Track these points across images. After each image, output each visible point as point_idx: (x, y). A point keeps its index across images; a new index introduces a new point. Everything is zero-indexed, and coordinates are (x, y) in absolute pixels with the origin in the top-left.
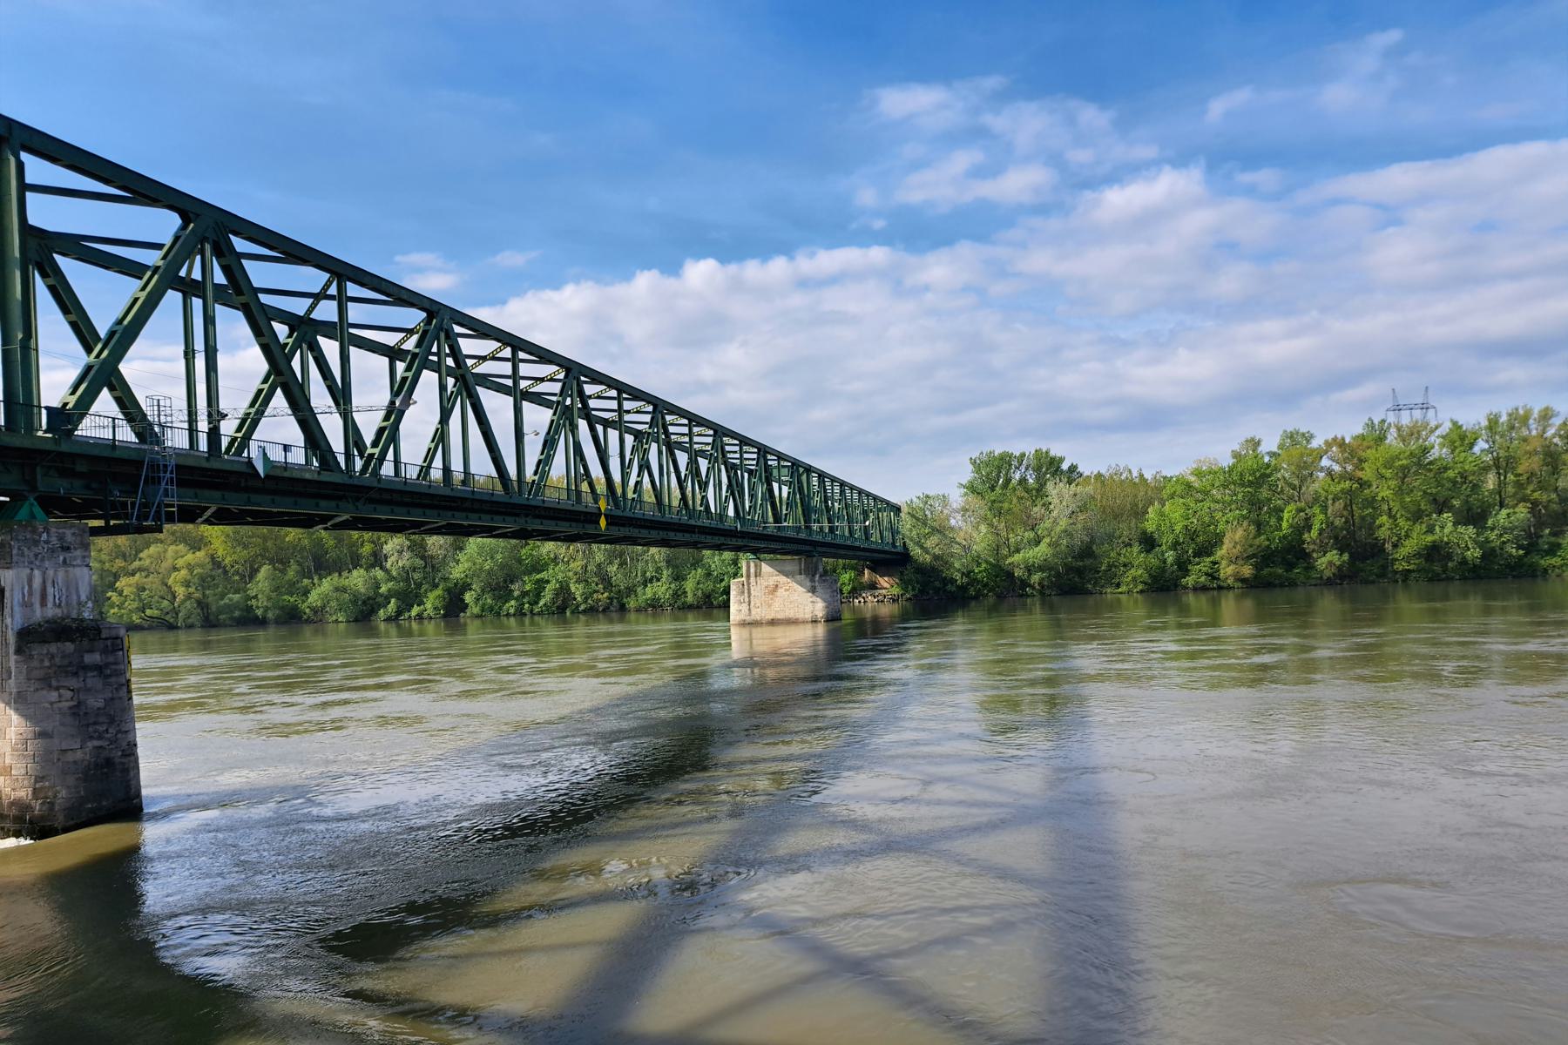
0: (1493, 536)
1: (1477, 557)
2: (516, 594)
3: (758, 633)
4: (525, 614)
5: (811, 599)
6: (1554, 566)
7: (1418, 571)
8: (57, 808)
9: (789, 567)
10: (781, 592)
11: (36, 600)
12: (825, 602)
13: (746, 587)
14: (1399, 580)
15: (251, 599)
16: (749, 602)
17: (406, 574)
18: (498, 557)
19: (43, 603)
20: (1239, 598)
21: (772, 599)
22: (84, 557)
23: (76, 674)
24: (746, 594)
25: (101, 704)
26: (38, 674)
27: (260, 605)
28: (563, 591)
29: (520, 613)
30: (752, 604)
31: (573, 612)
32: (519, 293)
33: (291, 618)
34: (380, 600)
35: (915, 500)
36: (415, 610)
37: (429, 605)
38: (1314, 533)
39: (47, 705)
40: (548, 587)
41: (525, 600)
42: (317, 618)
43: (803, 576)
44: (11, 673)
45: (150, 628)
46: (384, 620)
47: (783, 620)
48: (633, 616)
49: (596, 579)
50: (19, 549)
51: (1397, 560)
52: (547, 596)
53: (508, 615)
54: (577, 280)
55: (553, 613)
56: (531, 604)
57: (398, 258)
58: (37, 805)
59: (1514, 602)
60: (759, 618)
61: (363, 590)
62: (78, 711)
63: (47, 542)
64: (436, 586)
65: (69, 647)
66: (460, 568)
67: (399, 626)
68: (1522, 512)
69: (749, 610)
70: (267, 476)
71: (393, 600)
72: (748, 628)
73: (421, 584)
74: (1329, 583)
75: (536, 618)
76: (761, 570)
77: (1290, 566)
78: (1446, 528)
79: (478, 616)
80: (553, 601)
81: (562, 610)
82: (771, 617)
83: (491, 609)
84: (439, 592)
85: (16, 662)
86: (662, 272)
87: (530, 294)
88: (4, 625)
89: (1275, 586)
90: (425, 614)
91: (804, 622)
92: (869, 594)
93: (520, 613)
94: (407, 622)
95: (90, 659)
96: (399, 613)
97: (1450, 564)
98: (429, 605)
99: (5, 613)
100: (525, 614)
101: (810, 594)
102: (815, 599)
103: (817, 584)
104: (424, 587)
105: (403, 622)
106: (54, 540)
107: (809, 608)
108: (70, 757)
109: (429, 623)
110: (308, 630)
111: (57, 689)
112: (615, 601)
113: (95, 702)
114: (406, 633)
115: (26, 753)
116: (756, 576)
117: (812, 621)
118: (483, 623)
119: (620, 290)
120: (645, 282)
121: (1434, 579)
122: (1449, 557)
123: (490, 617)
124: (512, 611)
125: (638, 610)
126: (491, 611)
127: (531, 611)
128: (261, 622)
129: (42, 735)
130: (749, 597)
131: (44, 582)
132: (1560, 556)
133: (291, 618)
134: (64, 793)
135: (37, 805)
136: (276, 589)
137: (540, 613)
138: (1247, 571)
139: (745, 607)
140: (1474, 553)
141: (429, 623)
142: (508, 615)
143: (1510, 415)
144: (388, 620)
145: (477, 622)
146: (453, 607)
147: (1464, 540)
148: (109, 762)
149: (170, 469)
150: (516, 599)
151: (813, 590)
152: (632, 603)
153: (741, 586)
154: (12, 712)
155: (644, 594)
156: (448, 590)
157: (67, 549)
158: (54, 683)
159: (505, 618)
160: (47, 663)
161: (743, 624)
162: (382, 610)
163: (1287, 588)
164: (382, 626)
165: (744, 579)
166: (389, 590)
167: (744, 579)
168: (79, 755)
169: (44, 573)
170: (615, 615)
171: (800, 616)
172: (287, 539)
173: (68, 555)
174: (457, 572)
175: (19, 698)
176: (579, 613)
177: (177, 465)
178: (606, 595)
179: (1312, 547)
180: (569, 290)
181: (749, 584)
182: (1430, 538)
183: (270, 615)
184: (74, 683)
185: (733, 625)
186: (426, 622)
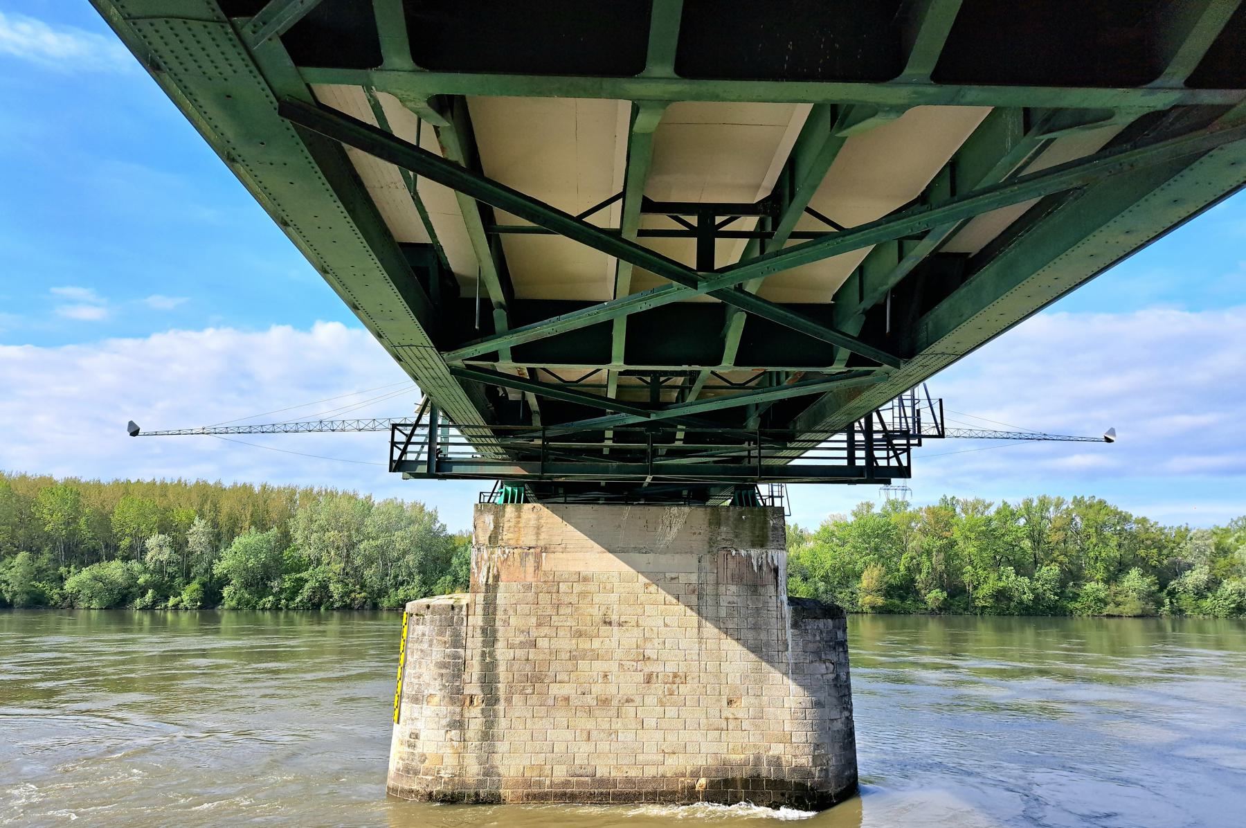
0: (1038, 585)
1: (1030, 600)
2: (274, 590)
4: (281, 609)
6: (1077, 609)
7: (991, 608)
8: (830, 774)
14: (978, 614)
17: (160, 569)
18: (262, 557)
20: (874, 619)
26: (811, 647)
27: (10, 589)
29: (276, 608)
31: (327, 609)
32: (163, 329)
33: (37, 603)
36: (172, 601)
38: (923, 575)
39: (819, 676)
40: (307, 586)
41: (283, 596)
42: (69, 604)
44: (788, 645)
46: (139, 609)
48: (385, 614)
51: (978, 598)
52: (306, 592)
53: (264, 609)
54: (217, 326)
55: (308, 609)
56: (287, 600)
57: (54, 290)
59: (1054, 631)
66: (224, 564)
67: (153, 616)
68: (1056, 569)
71: (150, 591)
73: (174, 577)
74: (932, 612)
75: (291, 613)
77: (903, 599)
78: (1009, 578)
79: (234, 609)
81: (317, 607)
83: (248, 603)
85: (793, 635)
86: (295, 328)
87: (171, 332)
88: (779, 601)
89: (895, 613)
90: (182, 605)
93: (276, 608)
94: (162, 612)
96: (155, 603)
97: (1012, 604)
98: (185, 597)
99: (779, 589)
100: (281, 609)
104: (177, 580)
105: (159, 611)
112: (369, 600)
115: (805, 721)
120: (278, 335)
121: (1001, 614)
122: (1010, 599)
124: (268, 605)
125: (389, 609)
127: (287, 606)
129: (818, 704)
132: (1080, 602)
133: (37, 603)
134: (833, 762)
135: (816, 772)
137: (294, 609)
138: (880, 601)
140: (1028, 597)
143: (1040, 501)
144: (144, 609)
145: (233, 615)
146: (210, 598)
147: (1022, 587)
150: (274, 595)
152: (385, 603)
154: (790, 682)
155: (397, 596)
158: (823, 657)
159: (260, 612)
162: (138, 600)
163: (903, 615)
164: (137, 615)
166: (146, 582)
170: (367, 613)
172: (46, 529)
174: (218, 569)
175: (796, 669)
179: (920, 585)
180: (209, 332)
182: (1001, 584)
183: (18, 599)
186: (181, 613)
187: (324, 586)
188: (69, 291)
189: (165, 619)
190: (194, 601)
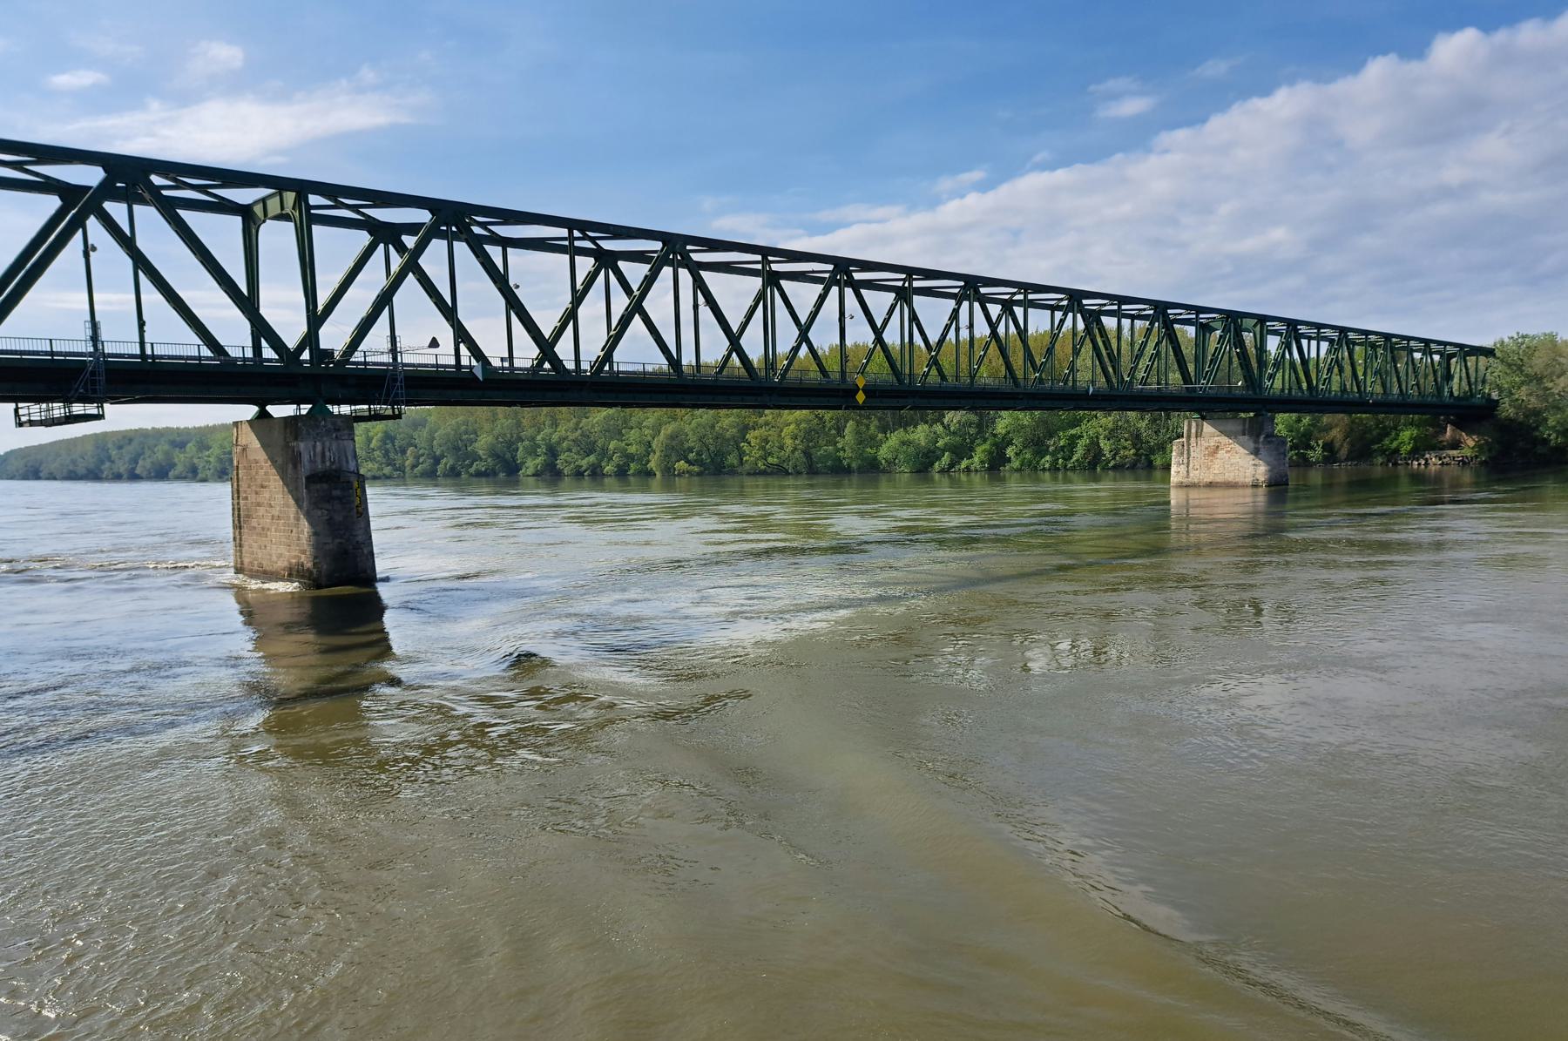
2: (1051, 449)
3: (1194, 494)
4: (1059, 469)
5: (1253, 462)
9: (1232, 426)
10: (1221, 453)
11: (319, 459)
12: (1268, 465)
13: (1186, 448)
15: (838, 450)
16: (1188, 463)
19: (323, 462)
21: (1212, 461)
22: (350, 435)
23: (328, 502)
24: (1185, 456)
25: (341, 519)
28: (1094, 449)
29: (1054, 468)
30: (1191, 466)
31: (1103, 469)
32: (1222, 106)
34: (938, 453)
35: (1506, 340)
37: (976, 459)
43: (1246, 437)
45: (772, 474)
46: (939, 472)
47: (1221, 483)
49: (1126, 435)
50: (307, 430)
53: (1044, 469)
54: (1291, 81)
55: (1085, 469)
57: (1092, 88)
58: (315, 571)
60: (1196, 481)
61: (923, 444)
62: (330, 522)
63: (325, 426)
64: (985, 440)
65: (325, 486)
67: (950, 476)
69: (1188, 472)
70: (484, 379)
71: (947, 454)
72: (1185, 489)
75: (1068, 473)
76: (1202, 430)
79: (1019, 470)
80: (1084, 457)
81: (1093, 465)
82: (1209, 480)
84: (986, 446)
91: (1244, 486)
92: (1433, 455)
93: (1054, 468)
95: (336, 493)
96: (952, 465)
100: (1059, 469)
101: (1252, 456)
102: (1257, 461)
103: (1261, 446)
106: (329, 426)
107: (1250, 471)
108: (327, 547)
109: (976, 474)
110: (883, 478)
111: (321, 509)
112: (1143, 457)
113: (338, 518)
114: (954, 483)
116: (1197, 437)
117: (1253, 486)
118: (1021, 475)
119: (1344, 87)
120: (1378, 70)
123: (1028, 471)
124: (1047, 466)
126: (1029, 466)
128: (848, 471)
129: (315, 534)
130: (1188, 458)
131: (323, 449)
134: (325, 567)
135: (315, 571)
136: (860, 443)
139: (1183, 469)
141: (976, 474)
142: (1044, 469)
144: (942, 471)
145: (1017, 475)
146: (996, 462)
148: (346, 552)
149: (399, 380)
150: (1053, 454)
151: (1256, 452)
153: (1181, 447)
156: (995, 444)
157: (339, 430)
160: (316, 495)
161: (1181, 486)
164: (937, 476)
165: (1184, 440)
166: (946, 444)
167: (1184, 440)
168: (331, 546)
169: (323, 444)
170: (1142, 473)
171: (1240, 479)
173: (339, 434)
176: (1109, 469)
177: (405, 377)
178: (1132, 451)
181: (1189, 445)
183: (854, 465)
184: (328, 506)
185: (1173, 486)
186: (973, 474)
187: (1094, 443)
188: (1112, 84)
189: (959, 479)
190: (982, 462)
